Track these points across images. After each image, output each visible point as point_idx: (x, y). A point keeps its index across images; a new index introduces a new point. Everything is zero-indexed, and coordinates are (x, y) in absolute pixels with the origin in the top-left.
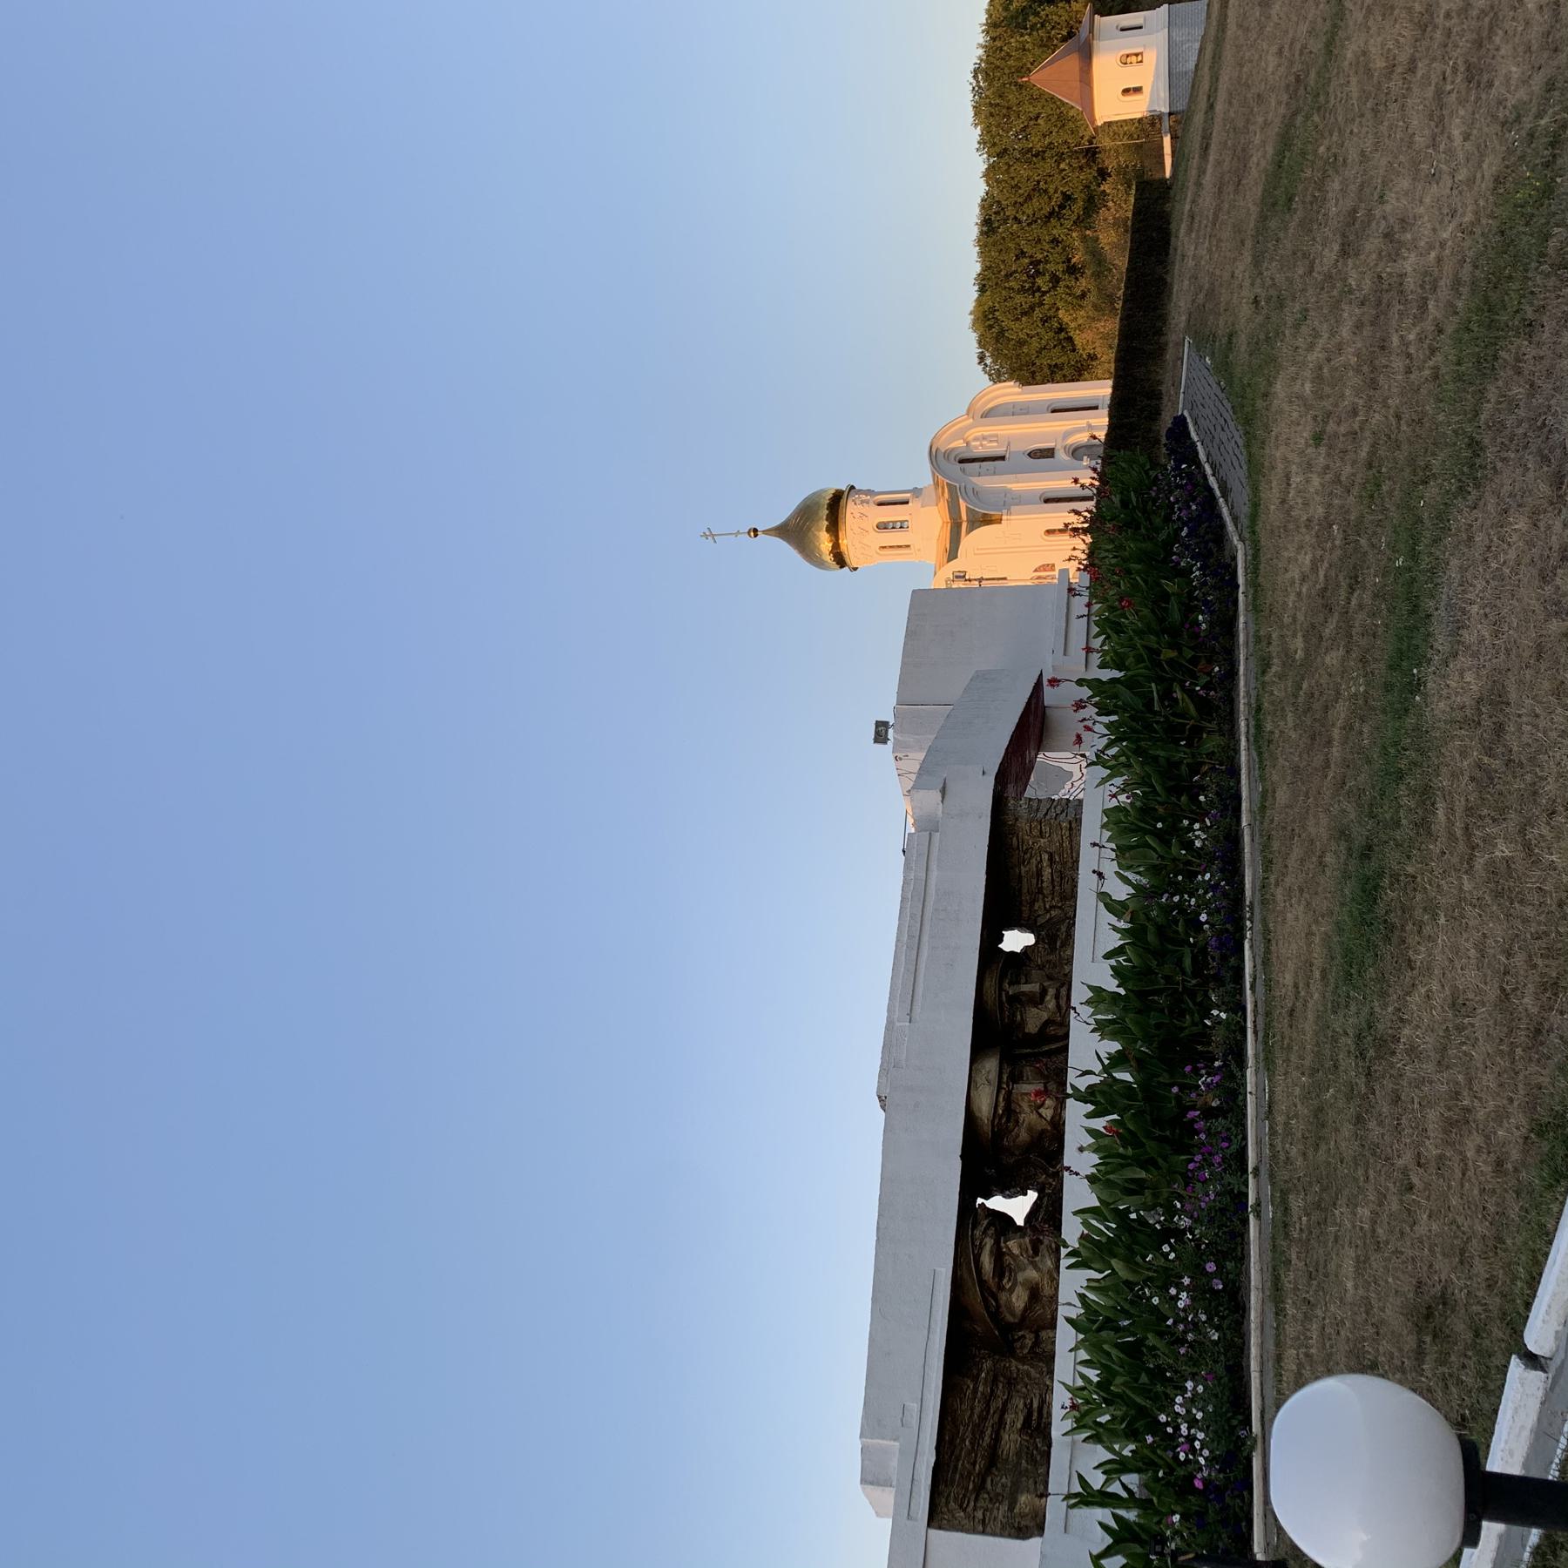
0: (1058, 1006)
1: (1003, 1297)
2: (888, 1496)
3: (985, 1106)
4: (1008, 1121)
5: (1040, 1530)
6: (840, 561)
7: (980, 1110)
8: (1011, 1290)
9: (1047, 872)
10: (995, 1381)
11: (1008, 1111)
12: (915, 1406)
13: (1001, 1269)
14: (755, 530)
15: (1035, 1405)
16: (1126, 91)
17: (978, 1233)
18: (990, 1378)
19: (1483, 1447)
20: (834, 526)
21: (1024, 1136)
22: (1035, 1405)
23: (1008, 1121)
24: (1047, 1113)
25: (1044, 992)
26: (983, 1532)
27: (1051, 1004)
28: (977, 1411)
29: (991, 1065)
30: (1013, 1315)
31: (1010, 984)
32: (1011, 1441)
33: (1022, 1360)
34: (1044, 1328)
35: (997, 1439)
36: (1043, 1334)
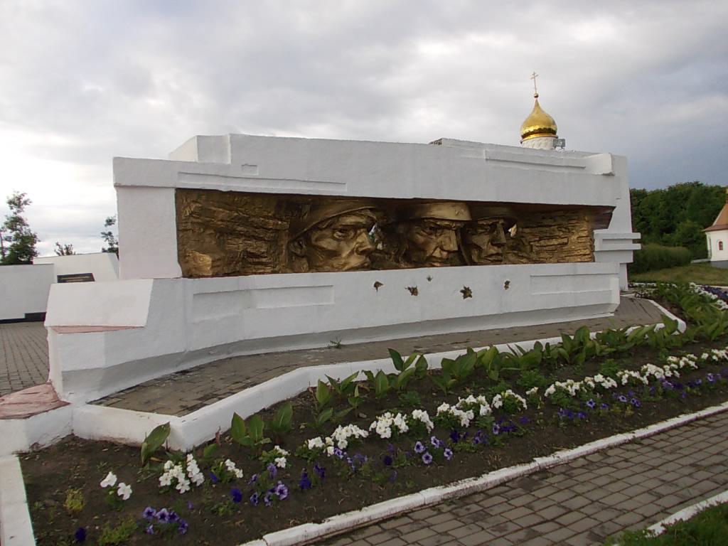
0: (492, 255)
1: (328, 233)
2: (191, 156)
3: (438, 212)
4: (431, 228)
5: (188, 274)
6: (524, 136)
7: (440, 209)
8: (333, 238)
9: (555, 242)
10: (277, 231)
11: (437, 227)
12: (256, 174)
13: (345, 230)
14: (537, 97)
15: (264, 260)
16: (721, 243)
17: (369, 213)
18: (278, 228)
19: (151, 409)
20: (540, 132)
21: (421, 239)
22: (264, 260)
23: (431, 228)
24: (437, 254)
25: (499, 245)
26: (178, 230)
27: (493, 250)
28: (255, 220)
29: (465, 216)
30: (317, 240)
31: (503, 224)
32: (238, 245)
33: (288, 248)
34: (309, 261)
35: (239, 235)
36: (304, 261)
